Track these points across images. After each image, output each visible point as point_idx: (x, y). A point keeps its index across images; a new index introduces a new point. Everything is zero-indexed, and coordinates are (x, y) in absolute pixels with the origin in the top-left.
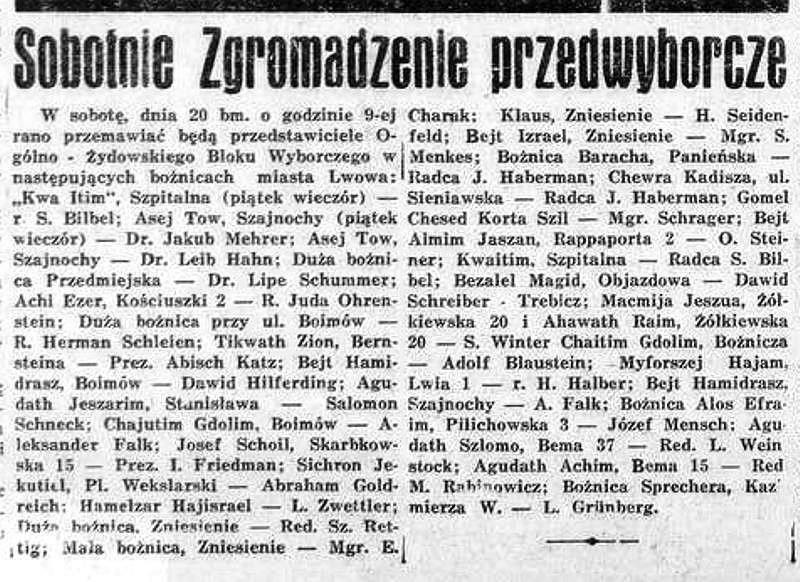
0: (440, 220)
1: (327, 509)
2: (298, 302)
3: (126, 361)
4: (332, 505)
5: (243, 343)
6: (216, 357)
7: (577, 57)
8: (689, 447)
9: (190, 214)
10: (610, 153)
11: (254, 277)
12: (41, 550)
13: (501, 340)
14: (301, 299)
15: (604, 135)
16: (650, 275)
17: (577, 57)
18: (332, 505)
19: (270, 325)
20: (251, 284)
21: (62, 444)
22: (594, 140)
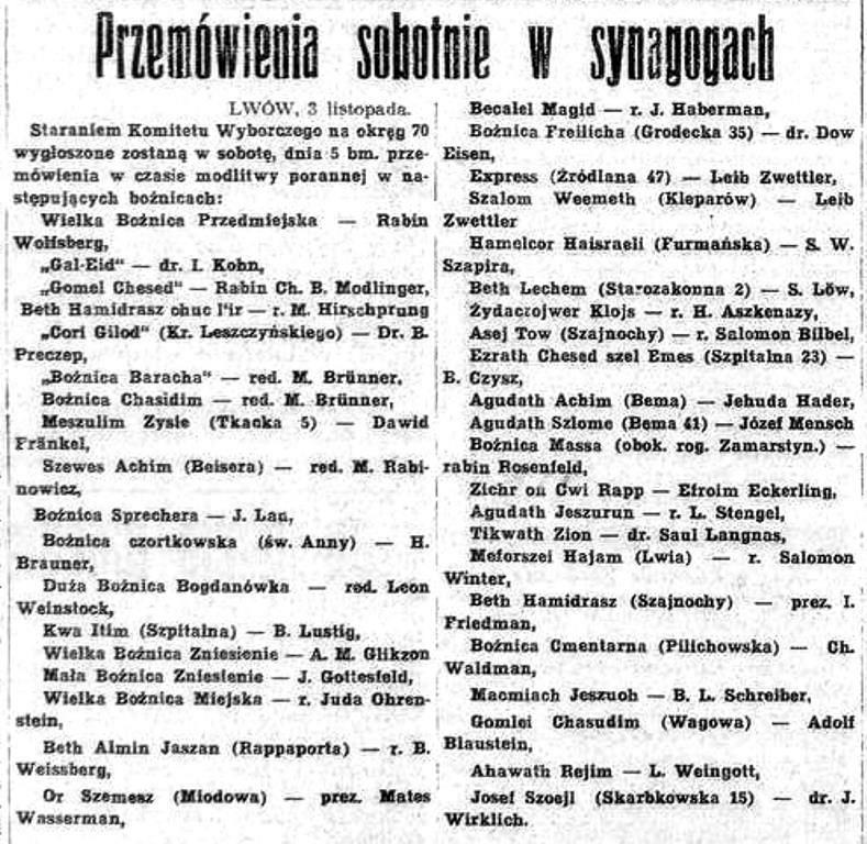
0: (588, 696)
1: (453, 224)
2: (330, 701)
3: (215, 219)
4: (458, 219)
5: (500, 534)
6: (499, 485)
7: (272, 54)
8: (275, 379)
9: (149, 418)
10: (451, 462)
11: (235, 106)
12: (217, 424)
13: (27, 607)
14: (333, 698)
15: (193, 674)
16: (132, 524)
17: (272, 54)
18: (458, 219)
19: (688, 539)
20: (232, 114)
21: (234, 585)
22: (183, 679)
